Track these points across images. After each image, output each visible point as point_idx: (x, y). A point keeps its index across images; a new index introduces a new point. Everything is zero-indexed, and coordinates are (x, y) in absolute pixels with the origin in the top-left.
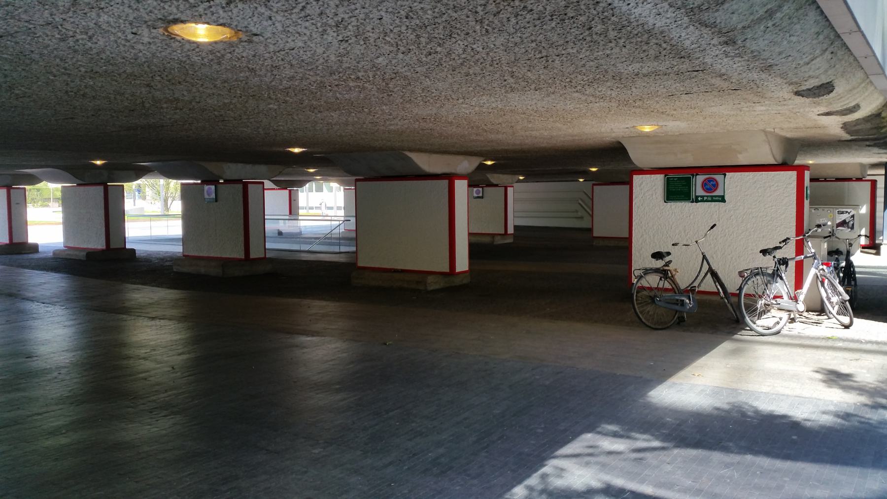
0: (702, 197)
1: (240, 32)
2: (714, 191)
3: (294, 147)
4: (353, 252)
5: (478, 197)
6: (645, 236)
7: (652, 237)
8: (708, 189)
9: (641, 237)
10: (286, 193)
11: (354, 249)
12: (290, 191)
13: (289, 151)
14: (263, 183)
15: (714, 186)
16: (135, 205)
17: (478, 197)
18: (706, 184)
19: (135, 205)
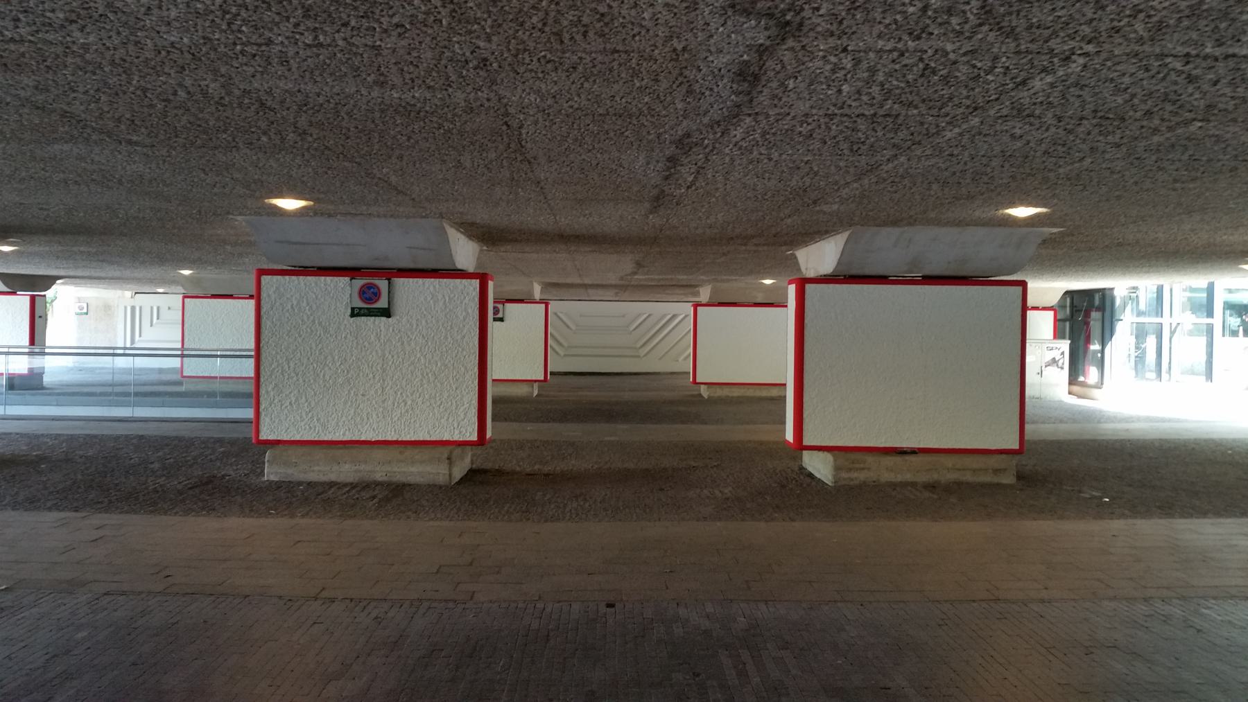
0: (360, 309)
1: (569, 607)
2: (376, 302)
3: (1013, 204)
4: (248, 422)
5: (81, 314)
6: (459, 337)
7: (449, 336)
8: (366, 298)
9: (464, 337)
10: (21, 301)
11: (249, 413)
12: (33, 299)
13: (1004, 215)
14: (1023, 284)
15: (375, 294)
16: (1160, 290)
17: (81, 314)
18: (364, 293)
19: (1160, 290)
